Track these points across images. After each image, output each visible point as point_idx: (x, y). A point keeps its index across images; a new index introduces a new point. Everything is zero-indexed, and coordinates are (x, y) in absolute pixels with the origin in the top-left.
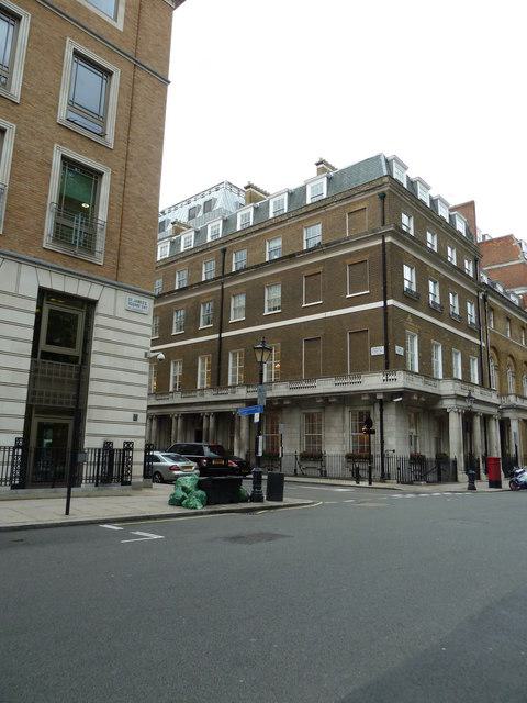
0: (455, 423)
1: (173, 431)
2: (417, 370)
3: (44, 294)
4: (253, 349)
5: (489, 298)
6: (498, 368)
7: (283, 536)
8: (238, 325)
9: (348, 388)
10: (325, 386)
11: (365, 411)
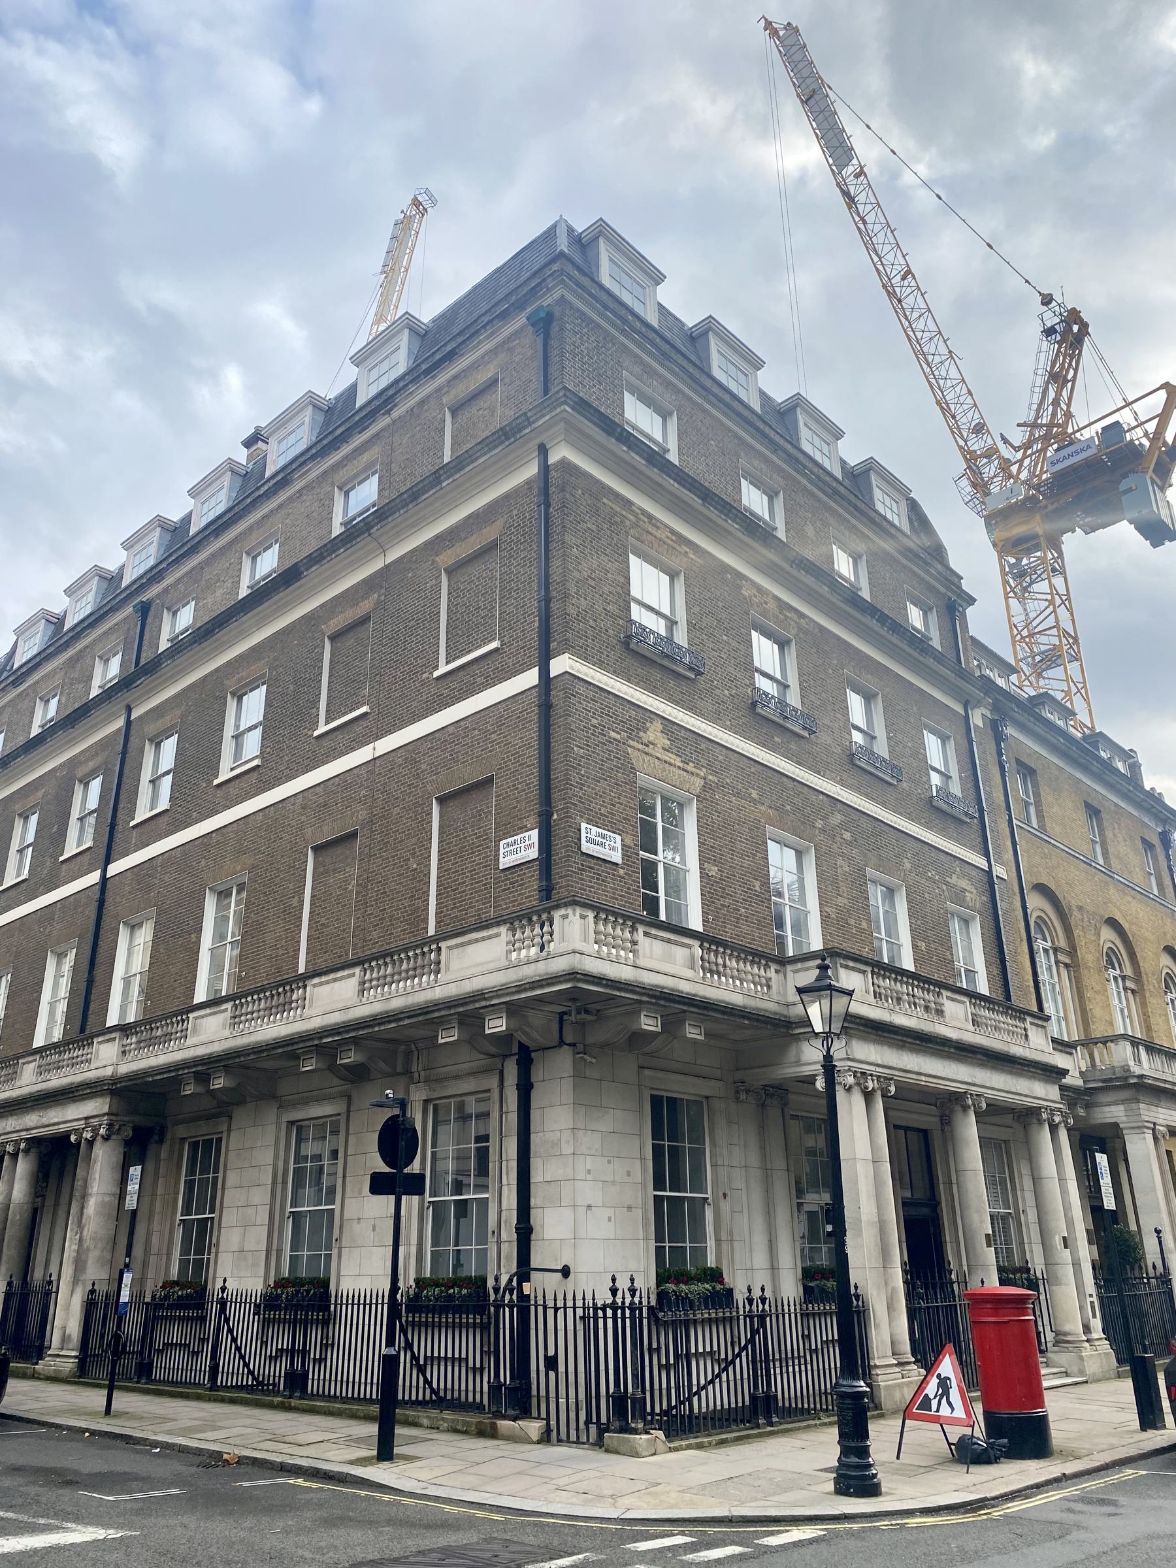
5: (1010, 730)
7: (821, 1470)
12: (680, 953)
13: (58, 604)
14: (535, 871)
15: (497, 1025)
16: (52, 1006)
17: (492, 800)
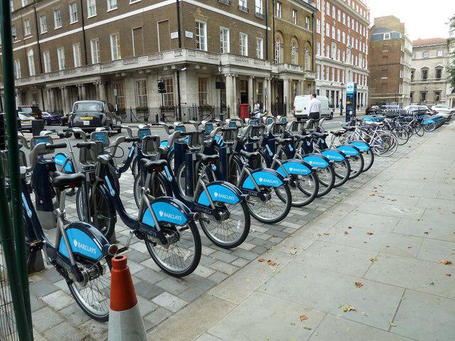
0: (230, 85)
1: (63, 98)
2: (206, 49)
4: (103, 35)
6: (283, 46)
8: (93, 20)
9: (156, 63)
10: (144, 62)
11: (165, 78)
15: (174, 68)
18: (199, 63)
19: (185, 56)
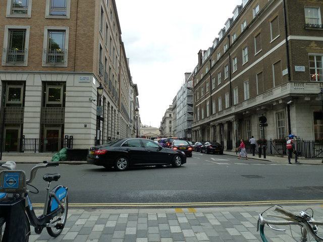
3: (45, 83)
8: (248, 64)
10: (260, 100)
12: (315, 86)
13: (218, 36)
14: (287, 76)
16: (246, 92)
17: (281, 63)
18: (308, 95)
19: (289, 89)
